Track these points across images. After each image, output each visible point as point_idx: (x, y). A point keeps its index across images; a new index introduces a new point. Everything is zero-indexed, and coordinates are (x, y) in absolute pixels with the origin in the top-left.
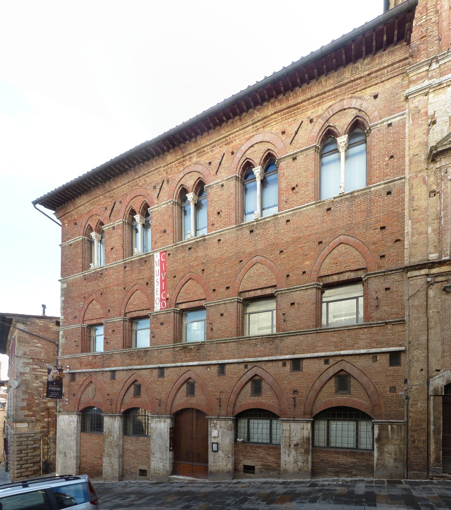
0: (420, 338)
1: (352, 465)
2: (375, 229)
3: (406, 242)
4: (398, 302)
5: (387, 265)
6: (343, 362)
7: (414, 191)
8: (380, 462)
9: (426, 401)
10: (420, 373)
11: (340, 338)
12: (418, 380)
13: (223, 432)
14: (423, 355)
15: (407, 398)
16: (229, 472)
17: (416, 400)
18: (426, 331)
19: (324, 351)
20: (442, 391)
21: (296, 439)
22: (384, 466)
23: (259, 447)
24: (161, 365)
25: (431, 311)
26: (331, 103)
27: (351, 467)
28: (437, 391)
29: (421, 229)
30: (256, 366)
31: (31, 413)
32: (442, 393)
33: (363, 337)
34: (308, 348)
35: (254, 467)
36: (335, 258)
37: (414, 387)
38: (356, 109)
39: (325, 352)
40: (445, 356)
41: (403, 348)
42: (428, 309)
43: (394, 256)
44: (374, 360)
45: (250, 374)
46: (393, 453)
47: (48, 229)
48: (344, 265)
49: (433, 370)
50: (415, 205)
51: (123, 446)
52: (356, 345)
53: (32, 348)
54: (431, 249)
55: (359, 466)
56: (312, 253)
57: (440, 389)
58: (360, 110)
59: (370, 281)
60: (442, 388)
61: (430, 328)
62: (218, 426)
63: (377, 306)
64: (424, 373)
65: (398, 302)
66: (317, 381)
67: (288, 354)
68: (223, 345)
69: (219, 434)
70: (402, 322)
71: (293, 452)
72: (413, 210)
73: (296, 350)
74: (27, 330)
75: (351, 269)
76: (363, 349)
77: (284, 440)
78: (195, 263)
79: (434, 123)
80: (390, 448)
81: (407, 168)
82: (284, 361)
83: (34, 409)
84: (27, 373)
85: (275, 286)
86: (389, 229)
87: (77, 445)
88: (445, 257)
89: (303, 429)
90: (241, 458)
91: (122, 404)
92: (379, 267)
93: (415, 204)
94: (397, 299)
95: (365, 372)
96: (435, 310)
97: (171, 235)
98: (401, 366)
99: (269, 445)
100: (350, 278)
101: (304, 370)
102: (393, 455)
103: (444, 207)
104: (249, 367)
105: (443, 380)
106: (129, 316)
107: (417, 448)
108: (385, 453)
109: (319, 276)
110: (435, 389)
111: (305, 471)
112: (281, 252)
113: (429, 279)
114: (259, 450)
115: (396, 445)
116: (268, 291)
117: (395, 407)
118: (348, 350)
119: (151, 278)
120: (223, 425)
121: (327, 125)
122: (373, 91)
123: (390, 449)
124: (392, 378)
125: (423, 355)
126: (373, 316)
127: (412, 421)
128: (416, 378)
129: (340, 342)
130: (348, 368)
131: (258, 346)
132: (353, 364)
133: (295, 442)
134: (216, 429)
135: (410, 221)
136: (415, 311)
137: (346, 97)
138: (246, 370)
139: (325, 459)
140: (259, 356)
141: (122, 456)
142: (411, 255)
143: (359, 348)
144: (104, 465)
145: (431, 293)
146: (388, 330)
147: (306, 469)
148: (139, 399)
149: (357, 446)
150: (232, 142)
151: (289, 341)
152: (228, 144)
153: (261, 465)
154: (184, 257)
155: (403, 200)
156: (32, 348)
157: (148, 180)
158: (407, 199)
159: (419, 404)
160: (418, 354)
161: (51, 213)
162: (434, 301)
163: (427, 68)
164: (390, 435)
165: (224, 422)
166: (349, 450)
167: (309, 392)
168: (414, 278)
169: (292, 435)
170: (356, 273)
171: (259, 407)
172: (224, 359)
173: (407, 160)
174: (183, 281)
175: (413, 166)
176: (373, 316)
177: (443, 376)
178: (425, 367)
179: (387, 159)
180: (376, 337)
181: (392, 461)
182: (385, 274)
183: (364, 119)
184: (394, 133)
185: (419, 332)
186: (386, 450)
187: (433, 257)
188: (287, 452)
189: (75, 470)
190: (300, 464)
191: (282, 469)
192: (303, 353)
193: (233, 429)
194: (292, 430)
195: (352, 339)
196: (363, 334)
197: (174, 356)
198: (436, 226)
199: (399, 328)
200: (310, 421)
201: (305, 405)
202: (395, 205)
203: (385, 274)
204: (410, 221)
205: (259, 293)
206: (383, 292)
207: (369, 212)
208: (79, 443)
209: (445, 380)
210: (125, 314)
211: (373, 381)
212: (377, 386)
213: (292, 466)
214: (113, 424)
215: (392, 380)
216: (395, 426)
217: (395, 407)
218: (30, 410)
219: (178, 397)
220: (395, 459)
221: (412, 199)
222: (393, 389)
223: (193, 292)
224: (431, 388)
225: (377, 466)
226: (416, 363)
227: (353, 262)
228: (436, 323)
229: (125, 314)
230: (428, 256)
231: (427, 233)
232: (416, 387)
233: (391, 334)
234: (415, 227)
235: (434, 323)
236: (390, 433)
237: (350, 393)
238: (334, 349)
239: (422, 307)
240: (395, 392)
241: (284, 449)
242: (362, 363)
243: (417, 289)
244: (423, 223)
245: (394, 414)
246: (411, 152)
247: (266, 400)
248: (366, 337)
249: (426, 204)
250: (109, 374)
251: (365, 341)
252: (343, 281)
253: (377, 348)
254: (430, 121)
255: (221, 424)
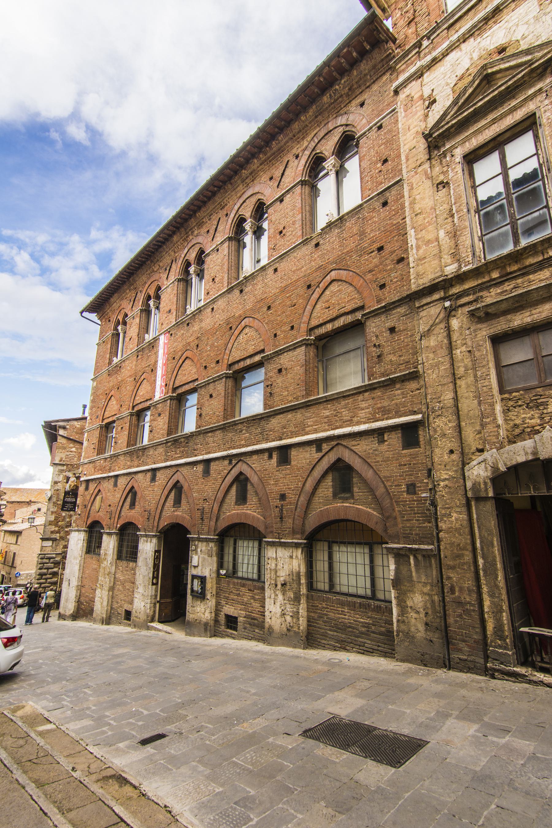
0: (442, 398)
1: (364, 629)
2: (372, 252)
3: (411, 259)
4: (407, 345)
5: (391, 295)
6: (340, 446)
7: (415, 192)
8: (403, 627)
9: (464, 509)
10: (449, 457)
11: (334, 410)
12: (447, 470)
13: (204, 559)
14: (450, 425)
15: (434, 504)
16: (206, 624)
17: (448, 508)
18: (451, 386)
19: (316, 431)
20: (486, 490)
21: (283, 575)
22: (408, 635)
23: (244, 586)
24: (154, 466)
25: (458, 351)
26: (315, 132)
27: (363, 633)
28: (479, 491)
29: (431, 236)
30: (240, 460)
31: (57, 529)
32: (487, 493)
33: (363, 404)
34: (297, 429)
35: (236, 618)
36: (327, 301)
37: (442, 484)
38: (342, 125)
39: (317, 433)
40: (487, 424)
41: (419, 416)
42: (454, 348)
43: (397, 281)
44: (380, 440)
45: (234, 472)
46: (422, 610)
47: (92, 329)
48: (337, 308)
49: (472, 451)
50: (417, 209)
51: (115, 575)
52: (355, 419)
53: (68, 453)
54: (447, 258)
55: (373, 632)
56: (301, 301)
57: (482, 486)
58: (347, 125)
59: (368, 324)
60: (485, 483)
61: (459, 378)
62: (199, 550)
63: (379, 356)
64: (454, 457)
65: (407, 345)
66: (309, 479)
67: (274, 441)
68: (210, 434)
69: (202, 562)
70: (414, 376)
71: (280, 597)
72: (416, 215)
73: (283, 434)
74: (65, 435)
75: (346, 311)
76: (365, 423)
77: (269, 575)
78: (191, 339)
79: (434, 101)
80: (417, 600)
81: (404, 167)
82: (270, 451)
83: (60, 523)
84: (59, 482)
85: (263, 351)
86: (388, 248)
87: (79, 570)
88: (465, 266)
89: (291, 557)
90: (223, 602)
91: (119, 517)
92: (379, 302)
93: (417, 207)
94: (406, 340)
95: (369, 461)
96: (464, 349)
97: (175, 313)
98: (420, 447)
99: (255, 583)
100: (346, 323)
101: (293, 463)
102: (422, 615)
103: (455, 200)
104: (234, 462)
105: (486, 468)
106: (136, 409)
107: (459, 603)
108: (409, 610)
109: (309, 327)
110: (474, 484)
111: (295, 632)
112: (269, 308)
113: (447, 304)
114: (243, 589)
115: (426, 594)
116: (257, 358)
117: (418, 520)
118: (345, 427)
119: (156, 362)
120: (204, 548)
121: (314, 153)
122: (359, 101)
123: (416, 602)
124: (409, 468)
125: (450, 425)
126: (376, 372)
127: (446, 548)
128: (443, 467)
129: (335, 416)
130: (347, 457)
131: (244, 432)
132: (353, 448)
133: (282, 579)
134: (196, 553)
135: (413, 230)
136: (431, 356)
137: (330, 119)
138: (231, 467)
139: (326, 615)
140: (244, 446)
141: (112, 589)
142: (418, 275)
143: (359, 423)
144: (96, 599)
145: (455, 323)
146: (397, 390)
147: (296, 629)
148: (133, 511)
149: (374, 591)
150: (226, 205)
151: (275, 422)
152: (223, 207)
153: (245, 617)
154: (183, 334)
155: (403, 207)
156: (68, 453)
157: (161, 264)
158: (407, 204)
159: (454, 515)
160: (441, 425)
161: (93, 316)
162: (461, 334)
163: (417, 50)
164: (414, 574)
165: (205, 544)
166: (359, 600)
167: (299, 497)
168: (425, 308)
169: (278, 567)
170: (353, 315)
171: (237, 521)
172: (209, 453)
173: (403, 158)
174: (181, 361)
175: (410, 162)
176: (376, 372)
177: (485, 460)
178: (455, 445)
179: (379, 165)
180: (381, 403)
181: (421, 627)
182: (387, 309)
183: (353, 131)
184: (385, 133)
185: (440, 388)
186: (409, 603)
187: (451, 269)
188: (273, 596)
189: (74, 605)
190: (288, 618)
191: (267, 625)
192: (291, 438)
193: (214, 554)
194: (279, 559)
195: (350, 409)
196: (363, 401)
197: (167, 452)
198: (449, 227)
199: (413, 385)
200: (301, 544)
201: (294, 518)
202: (394, 215)
203: (387, 309)
204: (413, 230)
205: (248, 362)
206: (387, 334)
207: (362, 234)
208: (82, 568)
209: (489, 468)
210: (133, 407)
211: (382, 475)
212: (388, 484)
213: (279, 621)
214: (109, 544)
215: (408, 471)
216: (420, 557)
217: (418, 520)
218: (56, 525)
219: (166, 508)
220: (427, 624)
221: (413, 203)
222: (412, 488)
223: (189, 373)
224: (469, 484)
225: (398, 635)
226: (441, 440)
227: (348, 301)
228: (466, 370)
229: (133, 407)
230: (442, 271)
231: (437, 239)
232: (447, 482)
233: (401, 397)
234: (420, 236)
235: (463, 369)
236: (413, 569)
237: (352, 497)
238: (327, 427)
239: (442, 348)
240: (415, 493)
241: (269, 591)
242: (363, 446)
243: (431, 322)
244: (430, 228)
245: (416, 534)
246: (407, 147)
247: (250, 512)
248: (367, 405)
249: (432, 202)
250: (113, 480)
251: (367, 410)
252: (338, 328)
253: (383, 420)
254: (427, 103)
255: (202, 547)
